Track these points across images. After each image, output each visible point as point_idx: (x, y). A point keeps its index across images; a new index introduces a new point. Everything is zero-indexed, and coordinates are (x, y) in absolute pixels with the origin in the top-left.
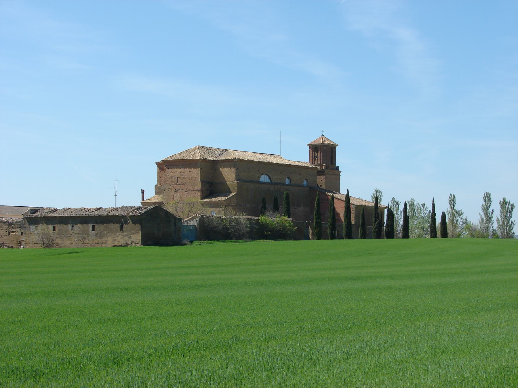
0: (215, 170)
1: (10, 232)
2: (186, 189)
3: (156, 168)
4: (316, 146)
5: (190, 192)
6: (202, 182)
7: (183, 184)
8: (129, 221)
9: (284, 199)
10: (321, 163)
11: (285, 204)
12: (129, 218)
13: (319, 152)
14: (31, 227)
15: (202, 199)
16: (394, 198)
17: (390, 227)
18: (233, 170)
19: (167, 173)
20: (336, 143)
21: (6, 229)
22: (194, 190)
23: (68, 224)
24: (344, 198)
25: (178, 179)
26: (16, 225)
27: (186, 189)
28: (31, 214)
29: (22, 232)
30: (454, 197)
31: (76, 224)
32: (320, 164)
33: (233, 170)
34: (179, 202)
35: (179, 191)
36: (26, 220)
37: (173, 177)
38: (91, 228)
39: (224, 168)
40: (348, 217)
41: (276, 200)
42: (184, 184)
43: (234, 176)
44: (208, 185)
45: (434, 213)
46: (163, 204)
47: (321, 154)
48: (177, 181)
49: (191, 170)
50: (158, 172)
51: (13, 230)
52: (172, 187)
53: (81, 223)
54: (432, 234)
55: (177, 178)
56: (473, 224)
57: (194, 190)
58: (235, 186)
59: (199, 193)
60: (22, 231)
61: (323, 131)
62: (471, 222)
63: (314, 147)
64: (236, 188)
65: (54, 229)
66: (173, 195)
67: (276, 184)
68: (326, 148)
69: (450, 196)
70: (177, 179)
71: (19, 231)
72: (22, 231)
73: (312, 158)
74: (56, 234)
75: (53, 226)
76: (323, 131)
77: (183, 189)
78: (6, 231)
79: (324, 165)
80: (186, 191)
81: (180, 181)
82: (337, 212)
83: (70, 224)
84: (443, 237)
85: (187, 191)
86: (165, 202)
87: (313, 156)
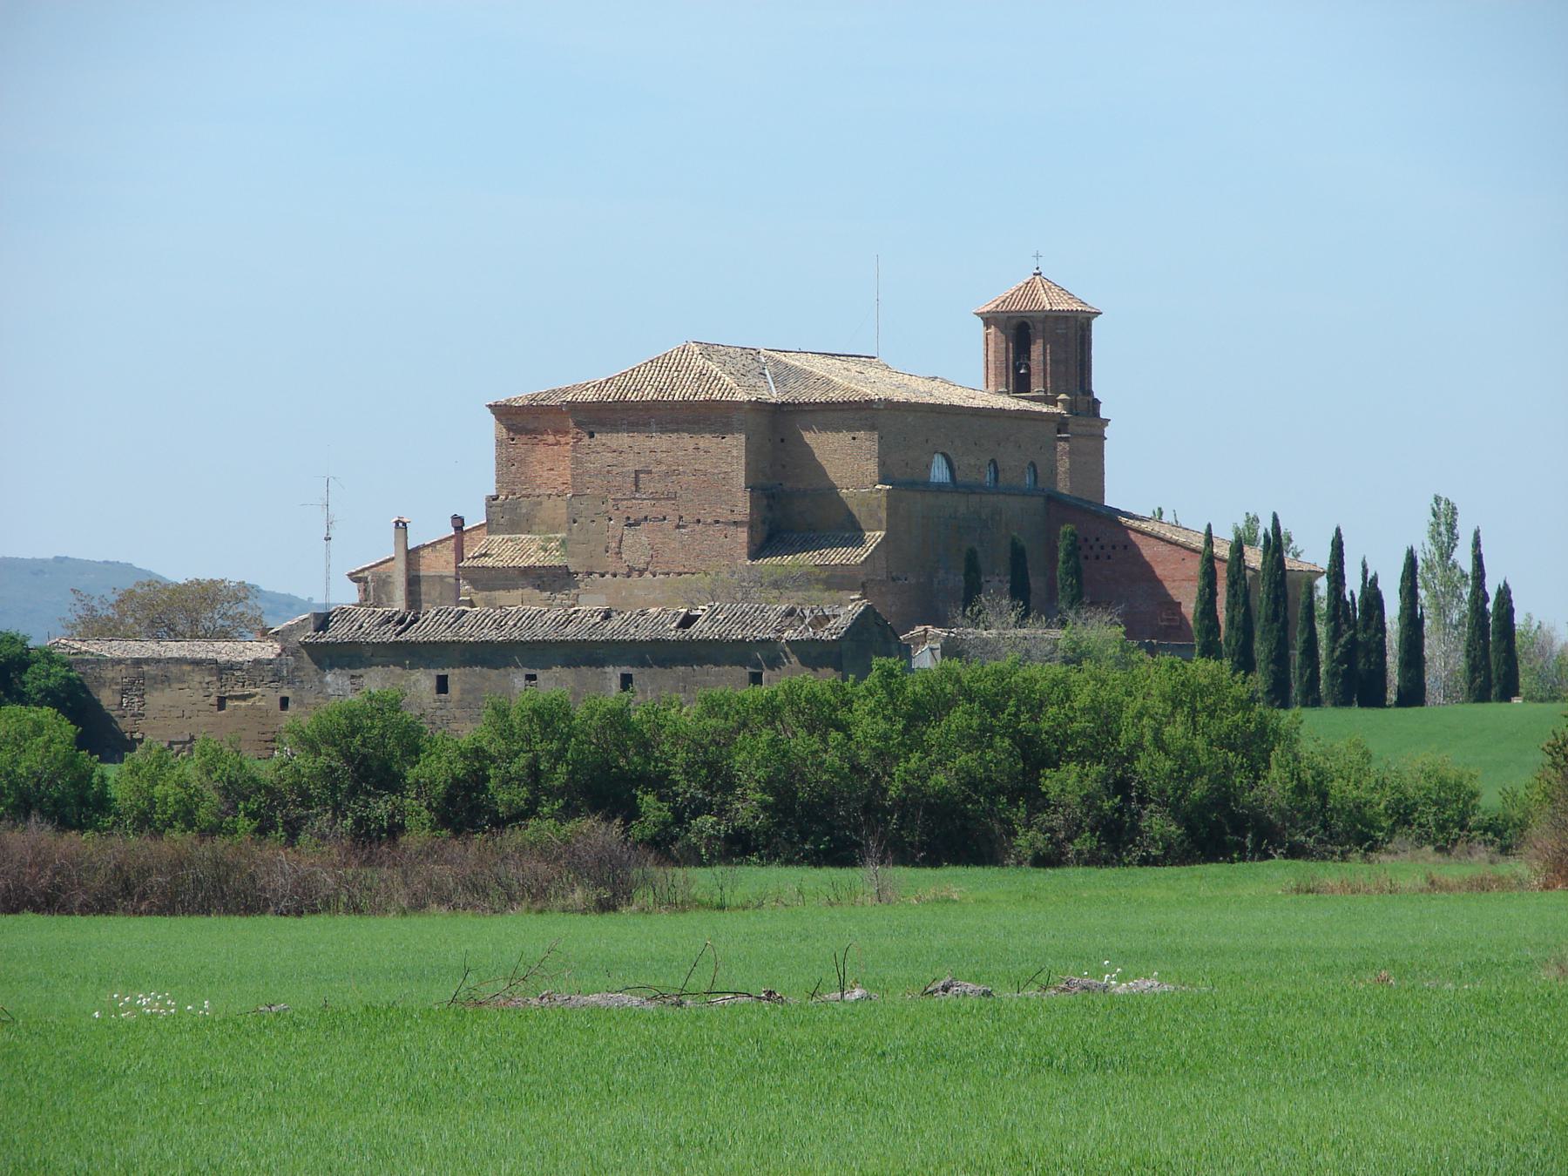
0: (782, 441)
1: (225, 698)
2: (681, 517)
3: (489, 427)
4: (1025, 319)
5: (699, 527)
6: (752, 487)
7: (668, 499)
8: (787, 658)
9: (1061, 555)
10: (1046, 392)
11: (1067, 574)
12: (787, 649)
13: (1040, 342)
14: (329, 678)
15: (754, 556)
16: (1160, 509)
17: (1374, 655)
18: (867, 442)
19: (587, 451)
20: (1093, 303)
21: (205, 685)
22: (717, 522)
23: (505, 666)
24: (1199, 543)
25: (641, 475)
26: (257, 673)
27: (681, 517)
28: (317, 630)
29: (287, 698)
30: (1454, 511)
31: (547, 666)
32: (1043, 394)
33: (867, 442)
34: (646, 569)
35: (644, 525)
36: (305, 655)
37: (615, 470)
38: (615, 683)
39: (819, 430)
40: (1281, 620)
41: (1018, 557)
42: (671, 497)
43: (872, 467)
44: (765, 502)
45: (1481, 592)
46: (569, 574)
47: (1045, 350)
48: (636, 485)
49: (701, 445)
50: (499, 443)
51: (238, 691)
52: (612, 510)
53: (569, 662)
54: (1477, 675)
55: (633, 475)
56: (1539, 627)
57: (717, 522)
58: (879, 507)
59: (743, 535)
60: (286, 695)
61: (1037, 256)
62: (1531, 618)
63: (1014, 321)
64: (883, 515)
65: (442, 685)
66: (617, 540)
67: (971, 489)
68: (1063, 326)
69: (1435, 505)
70: (637, 477)
71: (271, 693)
72: (286, 692)
73: (1007, 367)
74: (450, 705)
75: (622, 675)
76: (1037, 256)
77: (665, 519)
78: (207, 694)
79: (1062, 396)
80: (678, 527)
81: (649, 486)
82: (1169, 595)
83: (517, 667)
84: (1481, 694)
85: (684, 527)
86: (580, 567)
87: (1007, 359)
